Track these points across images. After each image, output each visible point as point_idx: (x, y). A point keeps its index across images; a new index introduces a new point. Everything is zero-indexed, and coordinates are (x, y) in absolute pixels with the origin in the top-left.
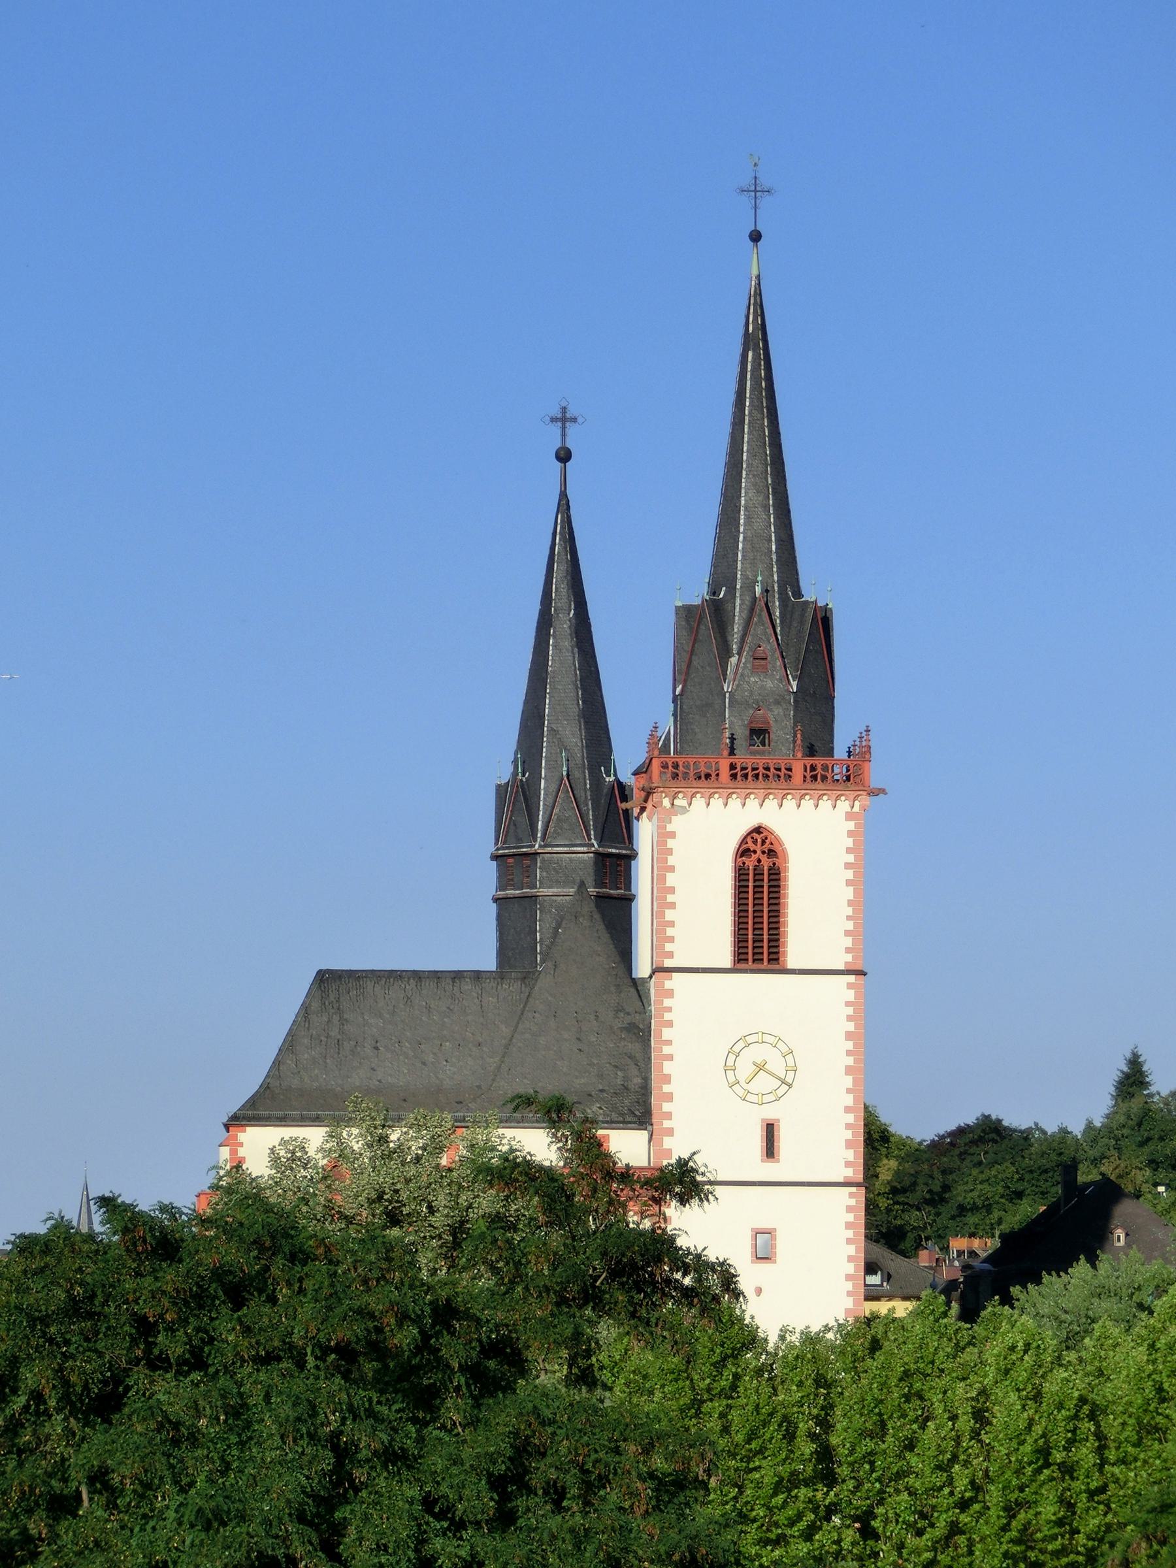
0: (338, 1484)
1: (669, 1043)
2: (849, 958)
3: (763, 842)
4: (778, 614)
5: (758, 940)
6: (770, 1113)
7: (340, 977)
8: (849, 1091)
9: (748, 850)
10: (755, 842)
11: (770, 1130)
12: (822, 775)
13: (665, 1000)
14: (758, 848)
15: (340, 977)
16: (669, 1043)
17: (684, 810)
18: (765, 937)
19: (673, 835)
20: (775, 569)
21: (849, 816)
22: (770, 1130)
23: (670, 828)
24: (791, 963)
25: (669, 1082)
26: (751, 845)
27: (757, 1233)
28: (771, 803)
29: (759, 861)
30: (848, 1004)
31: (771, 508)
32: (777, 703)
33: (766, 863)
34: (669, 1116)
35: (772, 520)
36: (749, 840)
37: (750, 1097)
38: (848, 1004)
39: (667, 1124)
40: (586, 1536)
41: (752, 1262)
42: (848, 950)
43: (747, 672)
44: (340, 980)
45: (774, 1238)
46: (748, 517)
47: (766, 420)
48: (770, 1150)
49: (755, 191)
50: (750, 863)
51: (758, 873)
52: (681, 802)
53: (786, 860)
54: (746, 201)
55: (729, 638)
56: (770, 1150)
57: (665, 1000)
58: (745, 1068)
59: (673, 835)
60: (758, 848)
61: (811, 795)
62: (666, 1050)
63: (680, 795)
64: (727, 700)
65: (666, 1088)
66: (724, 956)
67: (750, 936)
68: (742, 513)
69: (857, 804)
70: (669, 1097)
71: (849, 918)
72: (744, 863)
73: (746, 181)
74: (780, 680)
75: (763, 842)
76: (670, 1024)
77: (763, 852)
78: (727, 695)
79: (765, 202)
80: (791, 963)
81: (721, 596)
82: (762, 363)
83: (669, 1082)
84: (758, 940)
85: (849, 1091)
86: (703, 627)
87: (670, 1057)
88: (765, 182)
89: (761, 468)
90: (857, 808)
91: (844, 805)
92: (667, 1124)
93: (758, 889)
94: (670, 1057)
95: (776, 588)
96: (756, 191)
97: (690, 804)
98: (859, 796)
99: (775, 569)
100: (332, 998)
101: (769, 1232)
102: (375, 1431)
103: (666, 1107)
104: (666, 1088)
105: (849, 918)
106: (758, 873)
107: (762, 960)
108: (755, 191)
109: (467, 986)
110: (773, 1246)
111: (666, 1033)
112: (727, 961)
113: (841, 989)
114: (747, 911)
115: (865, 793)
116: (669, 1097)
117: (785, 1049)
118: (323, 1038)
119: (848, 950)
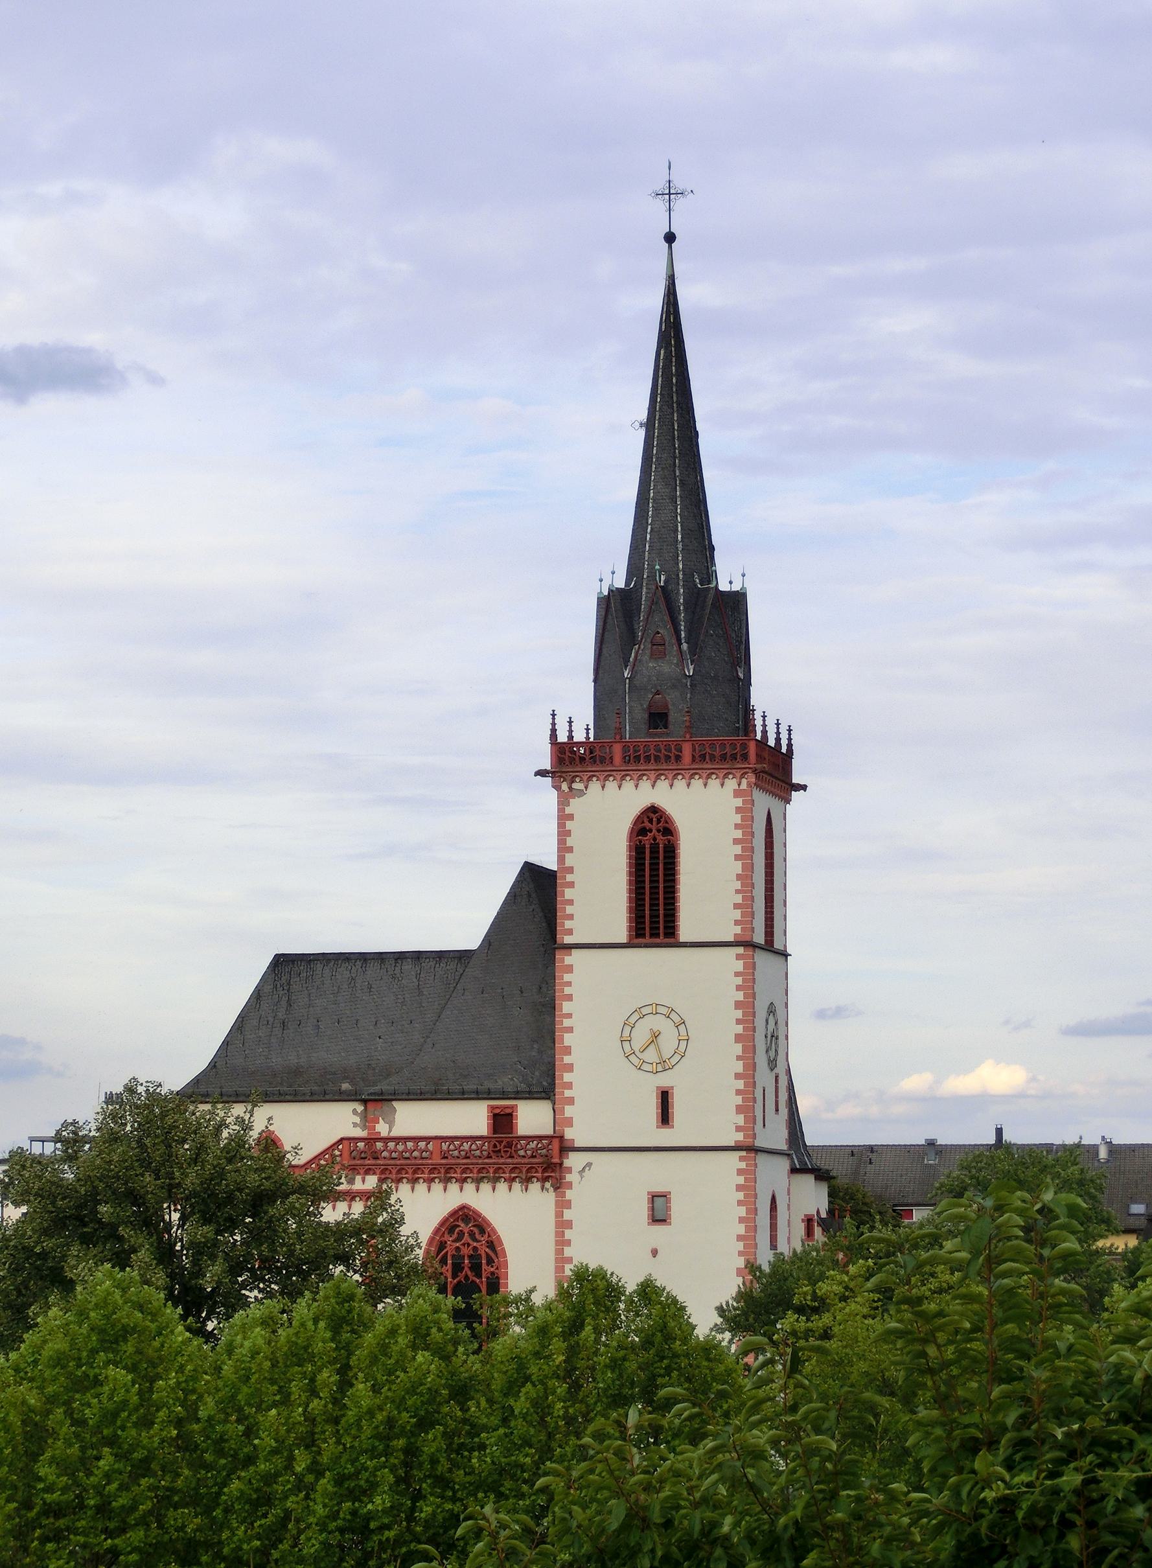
0: (335, 1464)
1: (569, 1016)
2: (738, 930)
3: (659, 821)
4: (682, 601)
5: (654, 916)
6: (664, 1080)
7: (293, 961)
8: (739, 1058)
9: (644, 828)
10: (651, 821)
11: (665, 1098)
12: (655, 756)
13: (565, 975)
14: (654, 827)
15: (293, 961)
16: (569, 1016)
17: (581, 793)
18: (662, 912)
19: (571, 817)
20: (680, 558)
21: (737, 793)
22: (665, 1098)
23: (568, 810)
24: (682, 939)
25: (570, 1054)
26: (647, 824)
27: (654, 1197)
28: (663, 784)
29: (655, 839)
30: (737, 974)
31: (678, 499)
32: (674, 687)
33: (661, 840)
34: (569, 1086)
35: (679, 511)
36: (646, 820)
37: (645, 1067)
38: (737, 974)
39: (568, 1093)
40: (141, 1353)
41: (649, 1224)
42: (737, 923)
43: (646, 658)
44: (293, 964)
45: (668, 1201)
46: (655, 509)
47: (675, 415)
48: (665, 1117)
49: (670, 194)
50: (647, 840)
51: (654, 849)
52: (578, 786)
53: (678, 839)
54: (661, 205)
55: (636, 626)
56: (665, 1117)
57: (565, 975)
58: (640, 1036)
59: (571, 817)
60: (654, 827)
61: (733, 774)
62: (567, 1023)
63: (578, 780)
64: (627, 686)
65: (567, 1059)
66: (620, 930)
67: (647, 912)
68: (651, 505)
69: (744, 781)
70: (570, 1068)
71: (737, 892)
72: (640, 842)
73: (661, 185)
74: (677, 665)
75: (659, 821)
76: (569, 998)
77: (659, 831)
78: (627, 681)
79: (679, 204)
80: (682, 939)
81: (632, 586)
82: (674, 359)
83: (570, 1054)
84: (654, 916)
85: (739, 1058)
86: (610, 617)
87: (570, 1030)
88: (679, 184)
89: (670, 462)
90: (744, 785)
91: (731, 784)
92: (568, 1093)
93: (654, 867)
94: (570, 1030)
95: (681, 576)
96: (670, 193)
97: (586, 788)
98: (746, 773)
99: (680, 558)
100: (283, 981)
101: (664, 1195)
102: (570, 1488)
103: (567, 1077)
104: (567, 1059)
105: (737, 892)
106: (654, 849)
107: (659, 934)
108: (670, 194)
109: (407, 966)
110: (668, 1209)
111: (566, 1007)
112: (622, 936)
113: (730, 961)
114: (644, 888)
115: (750, 771)
116: (570, 1068)
117: (677, 1019)
118: (270, 1018)
119: (737, 923)
